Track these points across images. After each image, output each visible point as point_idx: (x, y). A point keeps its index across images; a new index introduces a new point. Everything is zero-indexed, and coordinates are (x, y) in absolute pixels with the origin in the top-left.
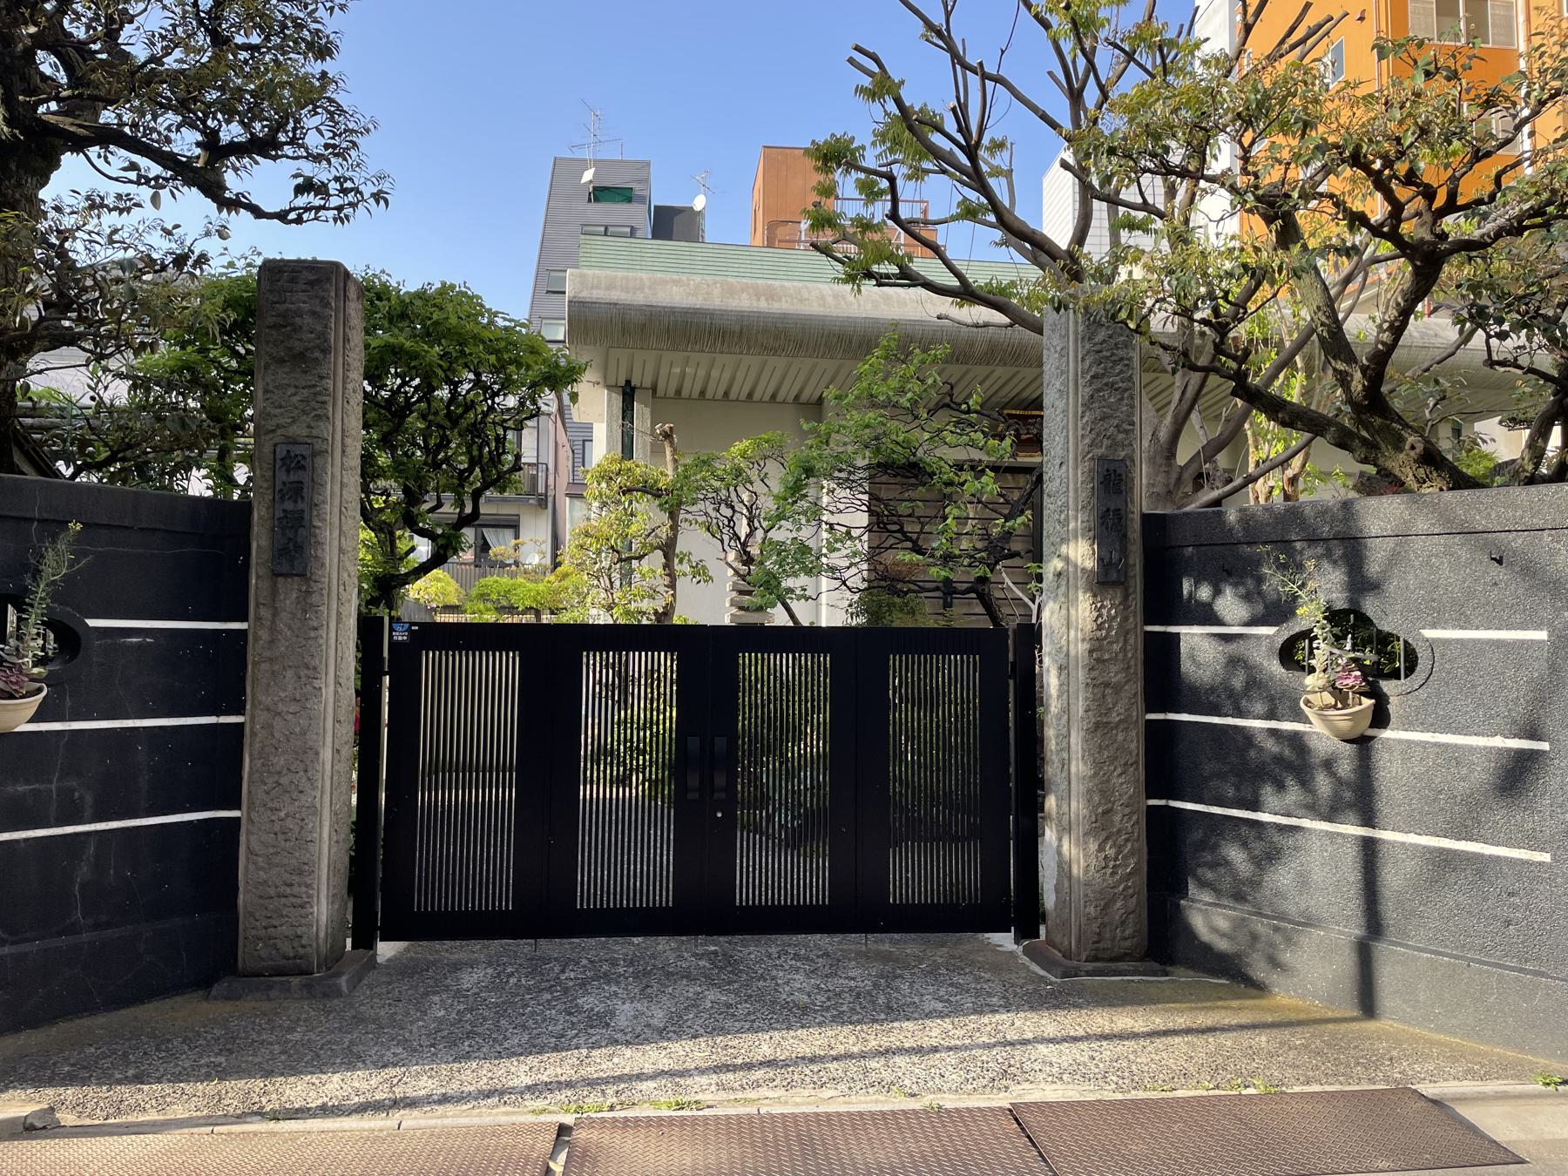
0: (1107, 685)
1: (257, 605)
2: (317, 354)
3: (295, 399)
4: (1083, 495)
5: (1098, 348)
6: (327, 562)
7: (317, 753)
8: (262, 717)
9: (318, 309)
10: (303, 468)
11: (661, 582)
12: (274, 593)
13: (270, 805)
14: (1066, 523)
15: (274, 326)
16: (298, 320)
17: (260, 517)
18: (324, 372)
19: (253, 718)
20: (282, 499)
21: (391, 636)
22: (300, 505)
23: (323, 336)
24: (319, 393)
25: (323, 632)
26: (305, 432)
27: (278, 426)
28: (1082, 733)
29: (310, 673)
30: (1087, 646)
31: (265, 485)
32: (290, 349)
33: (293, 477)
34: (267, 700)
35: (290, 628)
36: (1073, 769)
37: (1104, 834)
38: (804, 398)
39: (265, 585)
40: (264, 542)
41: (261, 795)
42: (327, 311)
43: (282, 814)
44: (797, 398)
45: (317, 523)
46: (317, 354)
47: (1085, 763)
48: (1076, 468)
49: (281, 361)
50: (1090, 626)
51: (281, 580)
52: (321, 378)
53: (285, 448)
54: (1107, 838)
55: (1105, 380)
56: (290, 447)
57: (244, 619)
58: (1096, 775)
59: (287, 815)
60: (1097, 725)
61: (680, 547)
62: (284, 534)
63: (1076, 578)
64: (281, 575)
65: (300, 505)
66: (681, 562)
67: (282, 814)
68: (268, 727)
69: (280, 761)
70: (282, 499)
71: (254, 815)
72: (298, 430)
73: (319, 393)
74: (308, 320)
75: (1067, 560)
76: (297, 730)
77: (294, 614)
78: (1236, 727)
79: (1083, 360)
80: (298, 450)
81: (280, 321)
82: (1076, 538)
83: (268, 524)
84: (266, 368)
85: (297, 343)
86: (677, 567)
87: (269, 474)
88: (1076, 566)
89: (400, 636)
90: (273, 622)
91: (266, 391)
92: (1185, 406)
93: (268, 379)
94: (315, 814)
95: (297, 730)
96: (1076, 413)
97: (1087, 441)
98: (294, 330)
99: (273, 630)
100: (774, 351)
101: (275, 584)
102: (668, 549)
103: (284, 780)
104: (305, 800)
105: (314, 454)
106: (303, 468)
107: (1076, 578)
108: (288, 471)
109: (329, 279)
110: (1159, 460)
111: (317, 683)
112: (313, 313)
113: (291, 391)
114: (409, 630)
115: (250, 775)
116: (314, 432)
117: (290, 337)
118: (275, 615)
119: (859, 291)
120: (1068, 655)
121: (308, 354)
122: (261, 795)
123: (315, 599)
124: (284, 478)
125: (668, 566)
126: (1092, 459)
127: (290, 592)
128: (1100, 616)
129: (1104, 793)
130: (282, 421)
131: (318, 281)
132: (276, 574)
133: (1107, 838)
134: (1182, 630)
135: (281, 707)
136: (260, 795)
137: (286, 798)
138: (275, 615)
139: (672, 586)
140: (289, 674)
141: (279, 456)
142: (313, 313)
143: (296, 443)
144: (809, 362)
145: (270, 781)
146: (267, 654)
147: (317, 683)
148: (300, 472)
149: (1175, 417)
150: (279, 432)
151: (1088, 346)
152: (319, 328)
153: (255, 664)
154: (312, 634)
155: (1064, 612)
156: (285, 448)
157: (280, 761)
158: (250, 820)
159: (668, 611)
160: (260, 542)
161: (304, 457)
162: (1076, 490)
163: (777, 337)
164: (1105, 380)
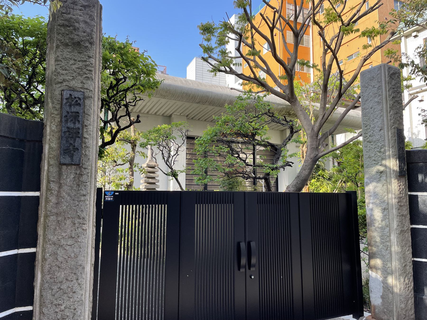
0: (403, 215)
1: (49, 182)
2: (87, 44)
3: (74, 67)
4: (392, 142)
5: (393, 87)
6: (91, 157)
7: (84, 268)
8: (50, 249)
9: (88, 21)
10: (79, 105)
11: (128, 173)
12: (60, 174)
13: (55, 302)
14: (384, 152)
15: (63, 25)
16: (77, 25)
17: (52, 131)
18: (91, 55)
19: (44, 250)
20: (67, 121)
21: (105, 198)
22: (77, 125)
23: (90, 35)
24: (88, 65)
25: (88, 197)
26: (80, 85)
27: (64, 80)
28: (396, 235)
29: (81, 221)
30: (397, 200)
31: (56, 112)
32: (72, 39)
33: (74, 109)
34: (53, 238)
35: (69, 195)
36: (393, 249)
37: (405, 274)
38: (165, 115)
39: (54, 170)
40: (54, 145)
41: (49, 296)
42: (93, 23)
43: (63, 308)
44: (163, 114)
45: (85, 135)
46: (87, 44)
47: (398, 247)
48: (388, 131)
49: (67, 45)
50: (397, 192)
51: (64, 167)
52: (90, 57)
53: (69, 92)
54: (406, 276)
55: (396, 99)
56: (72, 93)
57: (38, 189)
58: (402, 251)
59: (65, 308)
60: (402, 231)
61: (135, 161)
62: (67, 141)
63: (390, 174)
64: (64, 164)
65: (77, 125)
66: (135, 166)
67: (63, 308)
68: (55, 254)
69: (61, 275)
70: (67, 121)
71: (45, 310)
72: (76, 84)
73: (88, 65)
74: (82, 25)
75: (385, 166)
76: (73, 255)
77: (72, 187)
78: (415, 228)
79: (389, 91)
80: (76, 94)
81: (66, 23)
82: (390, 158)
83: (57, 135)
84: (58, 47)
85: (76, 37)
86: (134, 169)
87: (58, 106)
88: (390, 169)
89: (109, 198)
90: (59, 192)
91: (56, 60)
92: (324, 120)
93: (58, 54)
94: (82, 304)
95: (73, 255)
96: (387, 110)
97: (392, 121)
98: (75, 29)
99: (58, 196)
100: (164, 97)
101: (60, 169)
102: (131, 162)
103: (64, 287)
104: (76, 297)
105: (85, 98)
106: (79, 105)
107: (390, 174)
108: (70, 106)
109: (94, 6)
110: (314, 137)
111: (85, 227)
112: (86, 22)
113: (72, 62)
114: (114, 195)
115: (42, 285)
116: (86, 86)
117: (72, 33)
118: (60, 187)
119: (215, 75)
120: (388, 204)
121: (82, 43)
122: (49, 296)
123: (84, 178)
124: (68, 109)
125: (131, 168)
126: (394, 128)
127: (69, 174)
128: (400, 189)
129: (404, 258)
130: (67, 78)
131: (89, 6)
132: (61, 164)
133: (406, 276)
134: (419, 194)
135: (63, 242)
136: (48, 295)
137: (65, 297)
138: (60, 187)
139: (132, 175)
140: (68, 222)
141: (65, 97)
142: (86, 22)
143: (74, 90)
144: (174, 101)
145: (55, 288)
146: (54, 211)
147: (85, 227)
148: (77, 107)
149: (320, 123)
150: (65, 84)
151: (390, 86)
152: (88, 30)
153: (46, 217)
154: (83, 198)
155: (385, 187)
156: (69, 92)
157: (61, 275)
158: (41, 312)
159: (130, 185)
160: (50, 145)
161: (80, 99)
162: (389, 140)
163: (166, 92)
164: (396, 99)
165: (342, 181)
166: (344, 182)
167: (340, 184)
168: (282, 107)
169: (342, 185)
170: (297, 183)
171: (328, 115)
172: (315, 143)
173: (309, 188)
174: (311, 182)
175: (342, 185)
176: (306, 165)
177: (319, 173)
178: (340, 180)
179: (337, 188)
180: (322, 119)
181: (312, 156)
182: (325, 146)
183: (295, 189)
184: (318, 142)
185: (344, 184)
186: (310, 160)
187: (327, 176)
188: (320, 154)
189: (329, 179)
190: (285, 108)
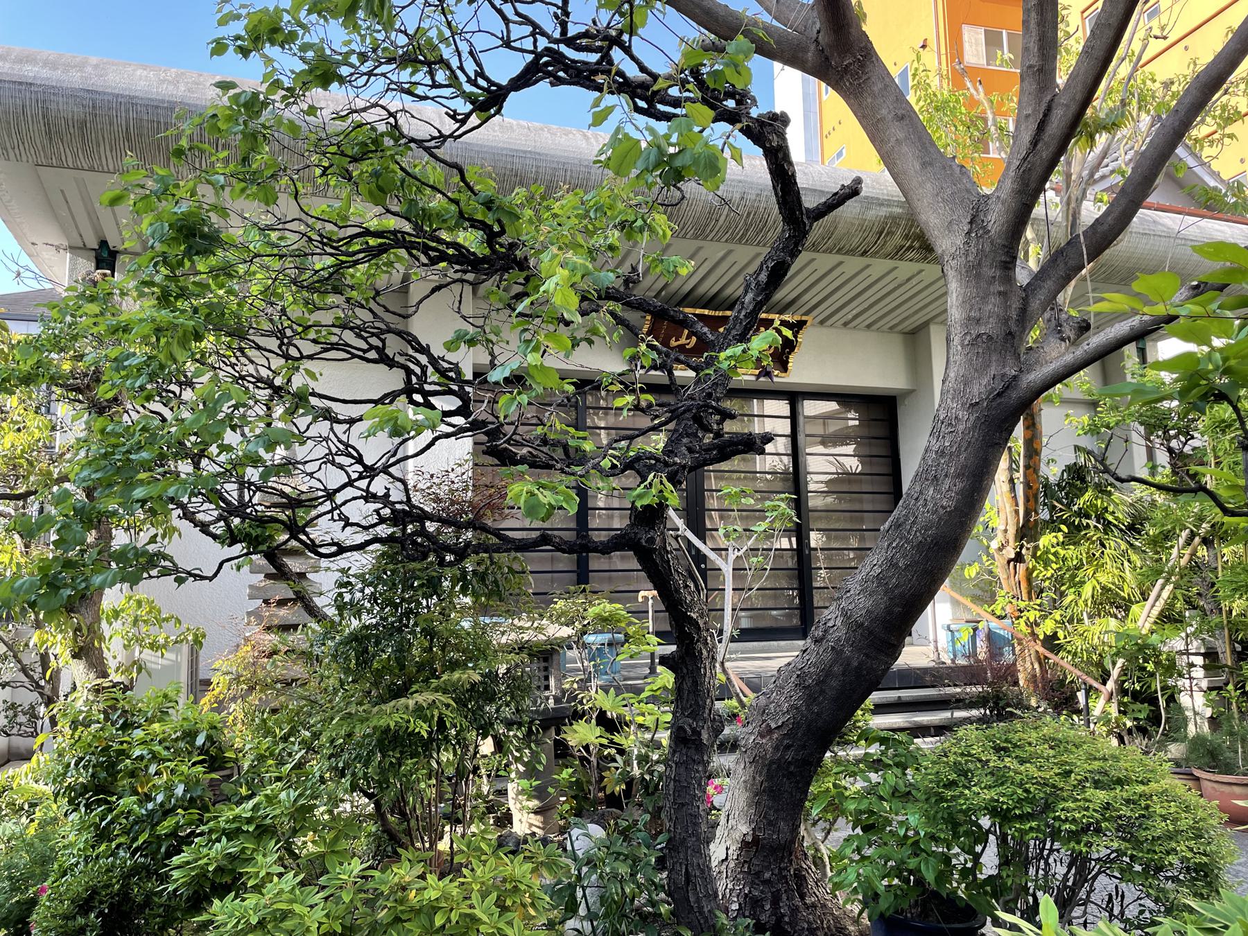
92: (1045, 153)
110: (988, 272)
165: (1193, 535)
166: (1206, 541)
167: (1187, 551)
168: (883, 212)
169: (1194, 554)
170: (892, 564)
171: (1074, 108)
172: (993, 306)
173: (1029, 572)
174: (1036, 548)
175: (1194, 554)
176: (941, 453)
177: (1081, 502)
178: (1185, 534)
179: (1171, 573)
180: (1035, 143)
181: (979, 389)
182: (1068, 332)
183: (881, 600)
184: (1015, 304)
185: (1202, 552)
186: (966, 419)
187: (1120, 514)
188: (1034, 377)
189: (1131, 527)
190: (899, 217)
